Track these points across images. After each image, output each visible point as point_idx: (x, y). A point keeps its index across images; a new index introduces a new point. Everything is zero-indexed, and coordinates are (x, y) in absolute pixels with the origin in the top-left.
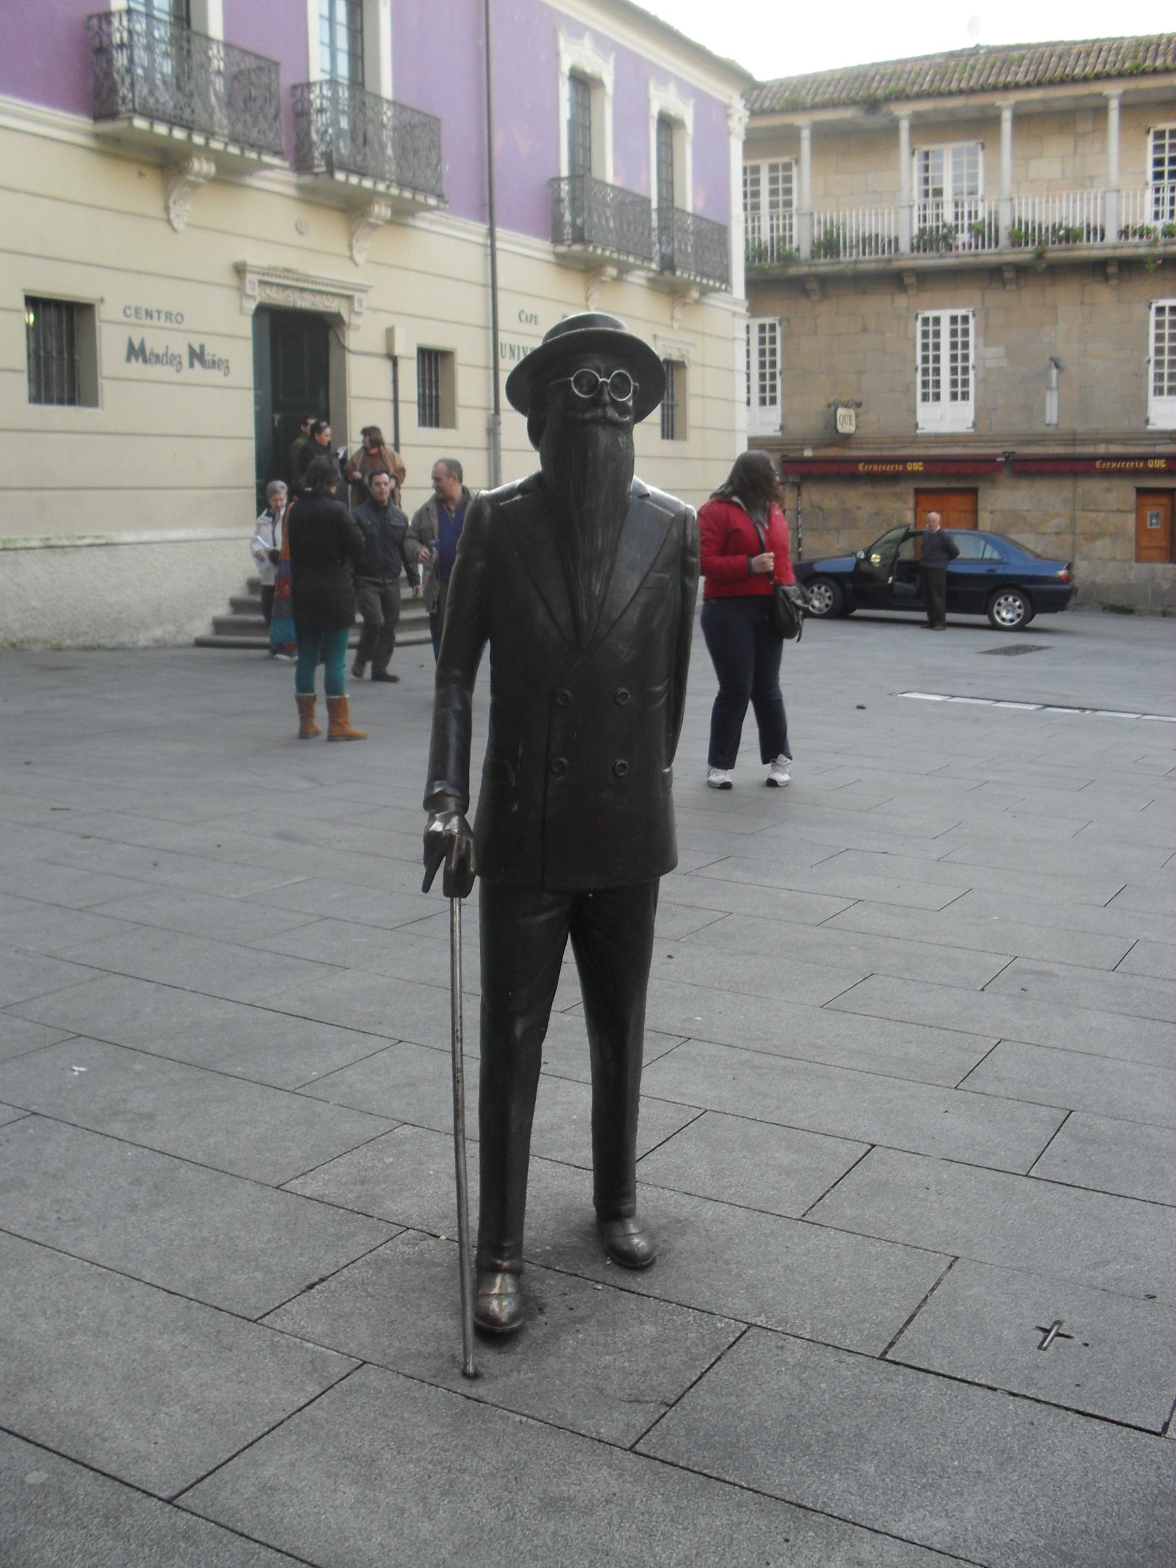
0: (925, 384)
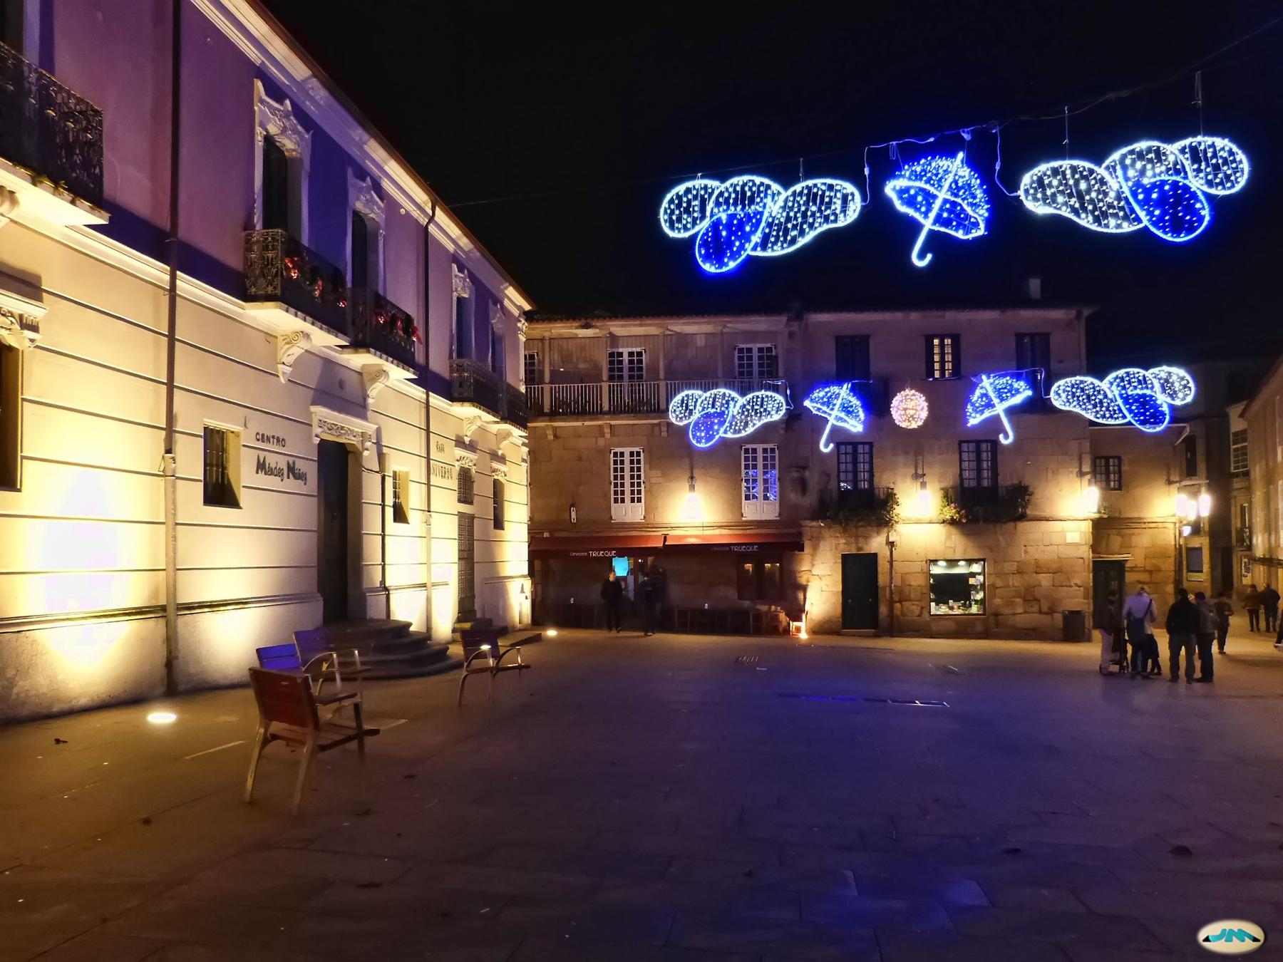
0: (616, 493)
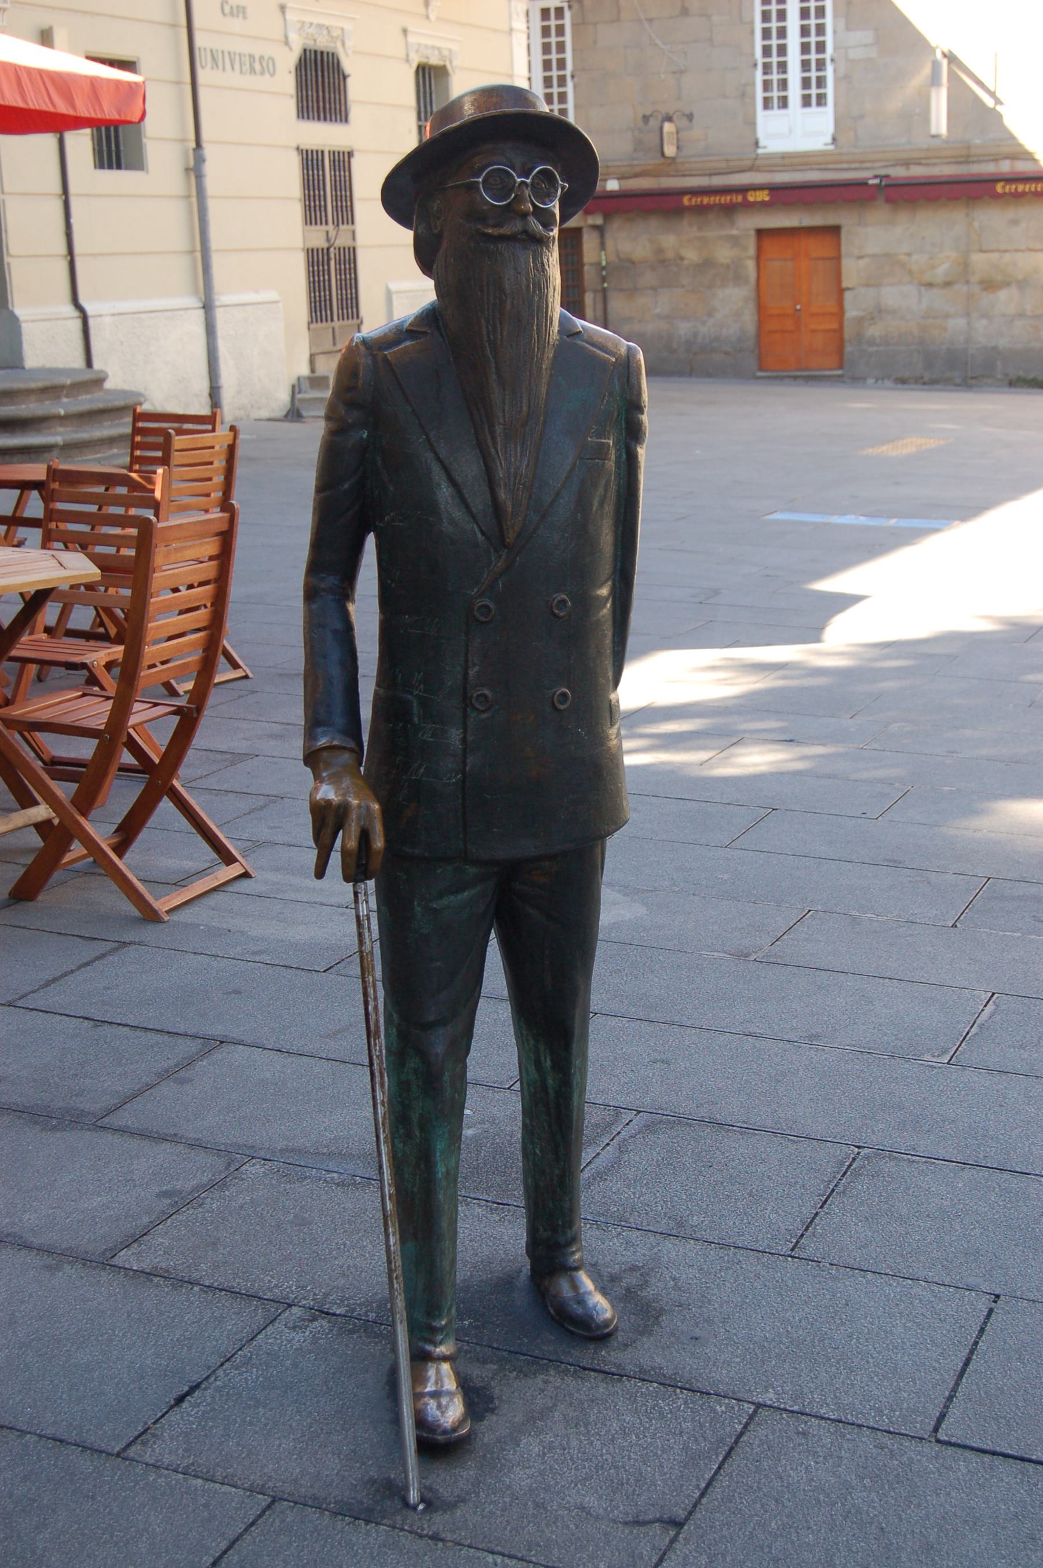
0: (767, 86)
